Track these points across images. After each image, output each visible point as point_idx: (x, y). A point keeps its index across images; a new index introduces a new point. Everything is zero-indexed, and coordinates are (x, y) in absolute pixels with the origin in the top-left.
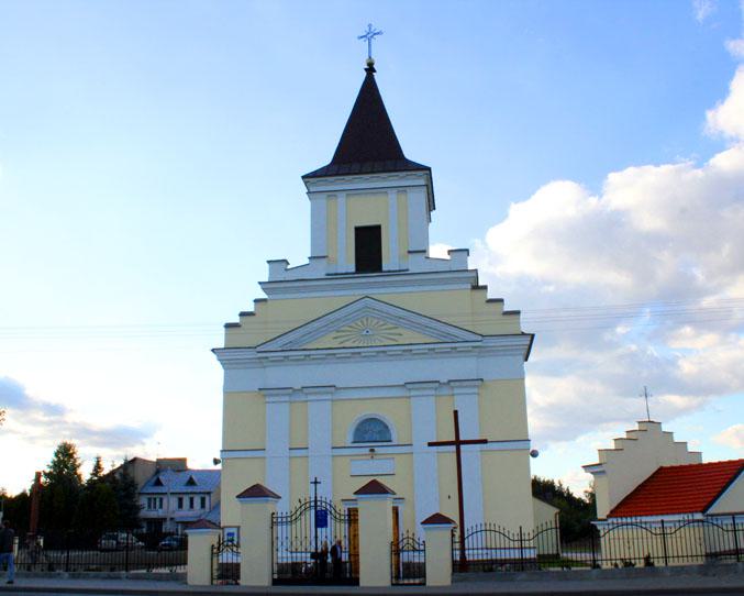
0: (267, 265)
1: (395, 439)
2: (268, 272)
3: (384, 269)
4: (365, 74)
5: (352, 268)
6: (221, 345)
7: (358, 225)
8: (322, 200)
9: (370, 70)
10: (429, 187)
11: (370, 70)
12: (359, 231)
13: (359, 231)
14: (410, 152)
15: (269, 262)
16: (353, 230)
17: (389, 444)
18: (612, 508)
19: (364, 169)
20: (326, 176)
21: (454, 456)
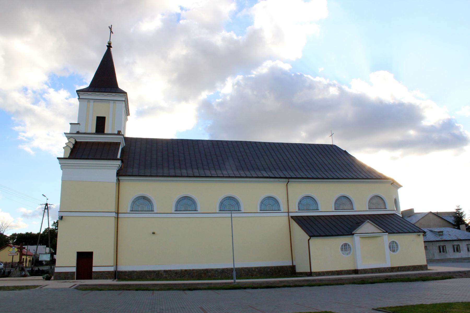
0: (70, 125)
1: (243, 209)
2: (69, 131)
3: (105, 132)
4: (106, 48)
5: (94, 131)
6: (62, 156)
7: (93, 252)
8: (85, 103)
9: (109, 46)
10: (127, 95)
11: (109, 46)
12: (98, 118)
13: (98, 118)
14: (121, 86)
15: (71, 124)
16: (92, 251)
17: (361, 236)
18: (431, 303)
19: (101, 91)
20: (88, 91)
21: (231, 220)
